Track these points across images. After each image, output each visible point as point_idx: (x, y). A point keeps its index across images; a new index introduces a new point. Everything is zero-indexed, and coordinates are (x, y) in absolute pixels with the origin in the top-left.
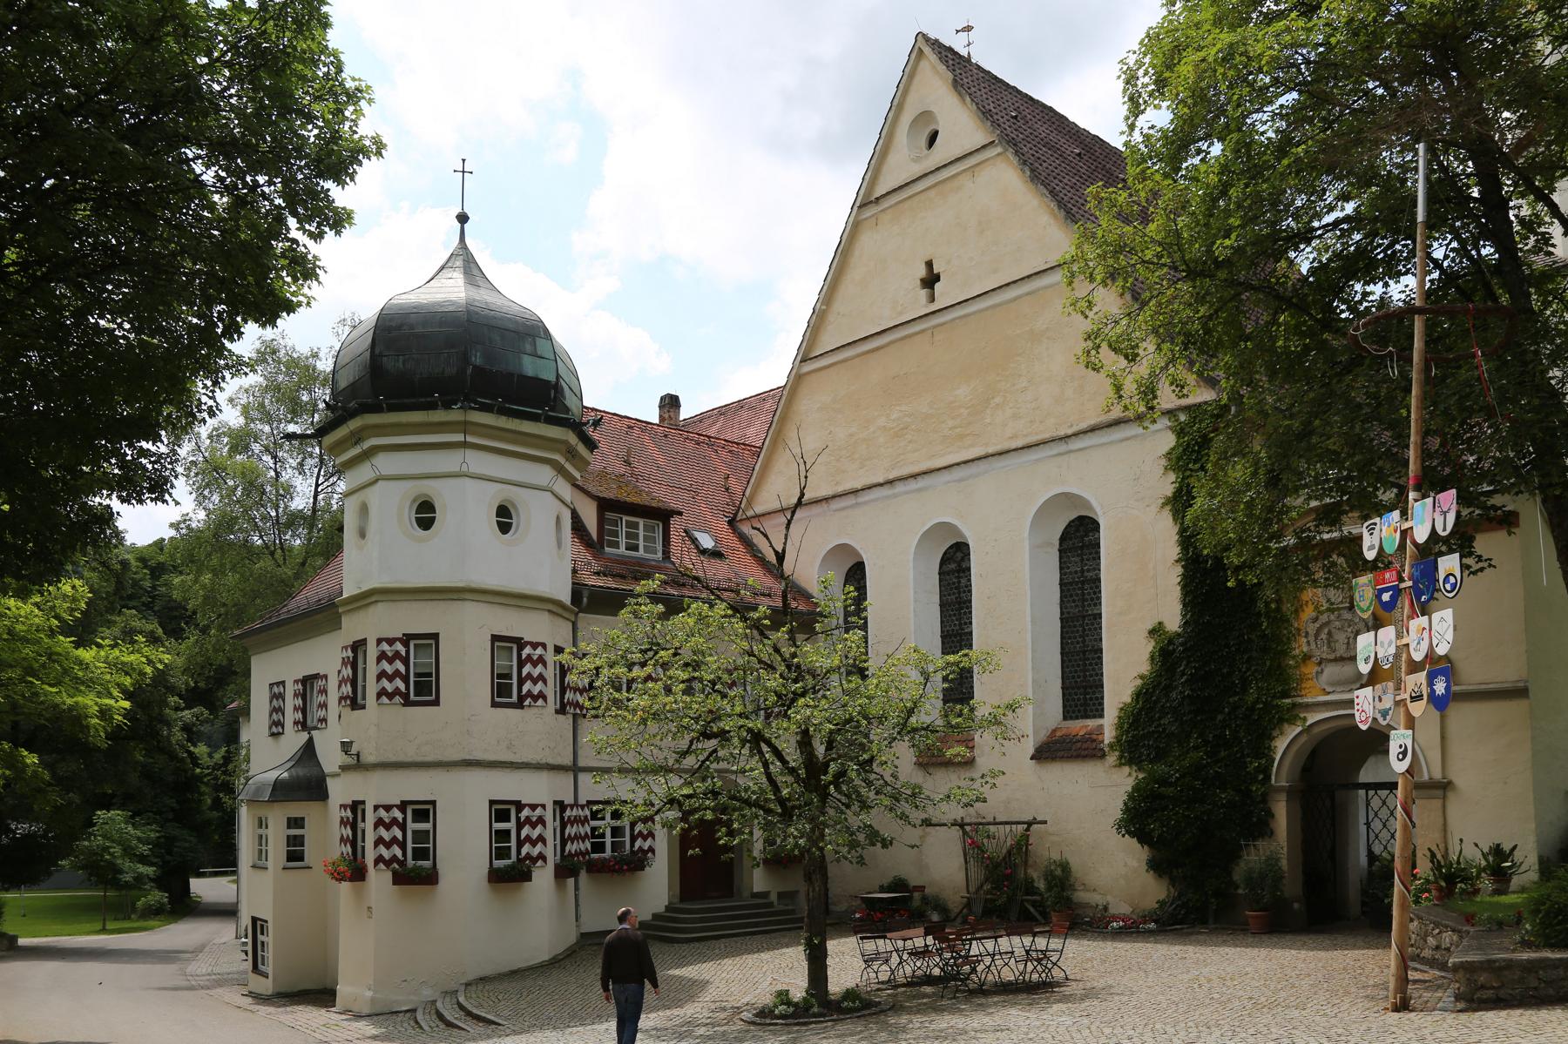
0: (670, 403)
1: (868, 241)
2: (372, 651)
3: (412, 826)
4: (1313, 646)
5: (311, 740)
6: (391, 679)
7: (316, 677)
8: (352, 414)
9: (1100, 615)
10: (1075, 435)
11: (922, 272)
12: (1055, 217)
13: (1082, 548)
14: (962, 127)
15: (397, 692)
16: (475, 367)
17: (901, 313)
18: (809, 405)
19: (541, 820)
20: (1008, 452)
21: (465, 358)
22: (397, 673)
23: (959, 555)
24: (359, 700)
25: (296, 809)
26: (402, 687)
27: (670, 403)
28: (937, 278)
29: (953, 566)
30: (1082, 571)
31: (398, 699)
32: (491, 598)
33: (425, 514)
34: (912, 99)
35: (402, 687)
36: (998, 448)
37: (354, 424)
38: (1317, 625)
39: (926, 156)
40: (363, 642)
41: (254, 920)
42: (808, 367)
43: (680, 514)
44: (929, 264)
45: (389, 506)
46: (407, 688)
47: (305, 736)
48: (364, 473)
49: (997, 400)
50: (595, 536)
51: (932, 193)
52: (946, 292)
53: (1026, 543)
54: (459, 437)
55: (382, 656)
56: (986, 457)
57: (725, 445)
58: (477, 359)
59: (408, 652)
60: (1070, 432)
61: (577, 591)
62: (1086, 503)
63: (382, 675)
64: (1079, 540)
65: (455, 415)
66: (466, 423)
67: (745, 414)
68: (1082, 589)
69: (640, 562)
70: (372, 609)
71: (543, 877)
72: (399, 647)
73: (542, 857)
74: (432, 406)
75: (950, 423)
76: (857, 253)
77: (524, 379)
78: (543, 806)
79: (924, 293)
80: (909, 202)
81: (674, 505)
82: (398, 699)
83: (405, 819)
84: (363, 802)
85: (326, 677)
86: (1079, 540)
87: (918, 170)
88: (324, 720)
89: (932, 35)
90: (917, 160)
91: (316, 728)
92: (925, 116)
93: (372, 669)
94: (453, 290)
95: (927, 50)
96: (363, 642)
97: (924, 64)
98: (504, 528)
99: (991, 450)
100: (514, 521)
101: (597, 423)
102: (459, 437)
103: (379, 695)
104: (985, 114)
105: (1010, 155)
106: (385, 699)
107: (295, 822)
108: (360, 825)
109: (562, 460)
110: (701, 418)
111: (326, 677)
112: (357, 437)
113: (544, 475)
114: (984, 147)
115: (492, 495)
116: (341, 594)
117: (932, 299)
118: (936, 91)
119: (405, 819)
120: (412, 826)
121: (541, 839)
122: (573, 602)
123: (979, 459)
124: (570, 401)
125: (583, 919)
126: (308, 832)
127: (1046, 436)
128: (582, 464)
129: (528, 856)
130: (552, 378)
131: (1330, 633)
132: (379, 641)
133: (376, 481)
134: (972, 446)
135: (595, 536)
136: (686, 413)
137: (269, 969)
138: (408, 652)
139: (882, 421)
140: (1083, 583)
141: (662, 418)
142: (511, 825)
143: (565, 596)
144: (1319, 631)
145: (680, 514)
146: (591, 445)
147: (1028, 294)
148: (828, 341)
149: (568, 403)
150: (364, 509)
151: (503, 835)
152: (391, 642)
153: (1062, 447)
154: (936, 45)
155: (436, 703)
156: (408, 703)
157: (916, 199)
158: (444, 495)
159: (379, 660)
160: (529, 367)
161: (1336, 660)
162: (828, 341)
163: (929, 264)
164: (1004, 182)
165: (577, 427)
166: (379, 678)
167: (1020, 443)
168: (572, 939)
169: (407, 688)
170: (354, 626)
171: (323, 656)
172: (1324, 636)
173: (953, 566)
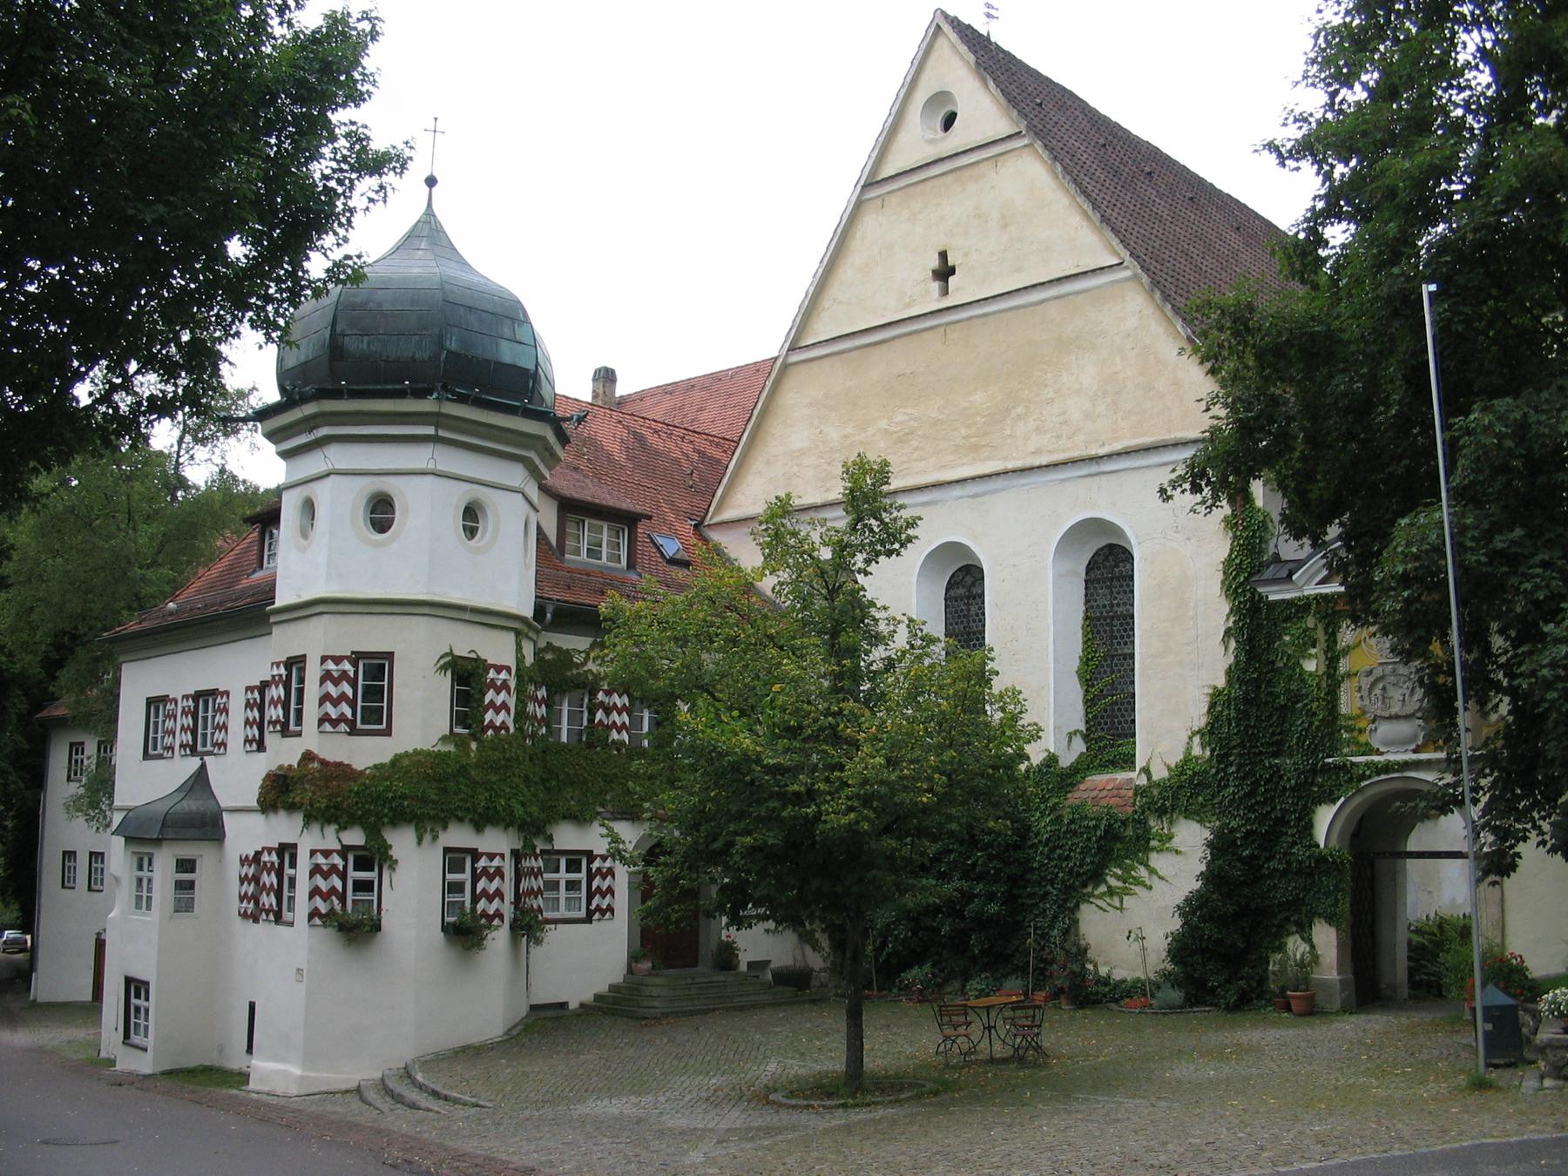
0: (606, 377)
1: (872, 225)
2: (313, 672)
3: (353, 875)
4: (1367, 702)
5: (203, 766)
6: (336, 703)
7: (213, 693)
8: (305, 399)
9: (1132, 656)
10: (1110, 456)
11: (935, 263)
12: (1088, 218)
13: (1112, 580)
14: (984, 114)
15: (342, 718)
16: (450, 352)
17: (908, 306)
18: (796, 397)
19: (499, 872)
20: (1031, 469)
21: (440, 342)
22: (343, 697)
23: (969, 579)
24: (292, 727)
25: (186, 851)
26: (348, 713)
27: (606, 377)
28: (952, 271)
29: (961, 591)
30: (1112, 605)
31: (343, 727)
32: (467, 616)
33: (381, 513)
34: (926, 77)
35: (348, 713)
36: (1019, 464)
37: (310, 409)
38: (1371, 679)
39: (943, 139)
40: (301, 659)
41: (129, 981)
42: (794, 358)
43: (650, 518)
44: (943, 255)
45: (340, 503)
46: (354, 714)
47: (195, 763)
48: (313, 464)
49: (1019, 410)
50: (553, 541)
51: (949, 179)
52: (962, 288)
53: (1050, 573)
54: (430, 430)
55: (326, 677)
56: (1006, 473)
57: (695, 436)
58: (453, 345)
59: (356, 672)
60: (1102, 452)
61: (539, 611)
62: (1118, 531)
63: (325, 698)
64: (1108, 568)
65: (427, 405)
66: (439, 414)
67: (697, 395)
68: (1111, 625)
69: (602, 572)
70: (314, 621)
71: (499, 939)
72: (347, 666)
73: (499, 915)
74: (400, 394)
75: (963, 431)
76: (859, 235)
77: (501, 366)
78: (502, 856)
79: (936, 286)
80: (921, 186)
81: (639, 509)
82: (343, 727)
83: (345, 867)
84: (295, 846)
85: (227, 693)
86: (1108, 568)
87: (932, 153)
88: (223, 744)
89: (952, 13)
90: (931, 142)
91: (210, 753)
92: (941, 97)
93: (312, 691)
94: (421, 268)
95: (946, 28)
96: (301, 659)
97: (941, 42)
98: (471, 532)
99: (1011, 465)
100: (480, 526)
101: (581, 420)
102: (430, 430)
103: (321, 721)
104: (1012, 100)
105: (1038, 145)
106: (327, 727)
107: (186, 865)
108: (288, 871)
109: (537, 461)
110: (641, 396)
111: (227, 693)
112: (309, 423)
113: (515, 475)
114: (1010, 137)
115: (460, 495)
116: (272, 600)
117: (945, 292)
118: (956, 74)
119: (345, 867)
120: (353, 875)
121: (499, 894)
122: (535, 617)
123: (998, 474)
124: (545, 392)
125: (533, 989)
126: (201, 877)
127: (1075, 454)
128: (551, 458)
129: (484, 914)
130: (531, 367)
131: (1384, 689)
132: (324, 659)
133: (328, 475)
134: (989, 458)
135: (553, 541)
136: (622, 389)
137: (150, 1042)
138: (356, 672)
139: (883, 424)
140: (1112, 618)
141: (595, 395)
142: (466, 876)
143: (528, 612)
144: (1373, 685)
145: (650, 518)
146: (563, 439)
147: (1057, 298)
148: (824, 328)
149: (544, 393)
150: (309, 507)
151: (456, 888)
152: (338, 660)
153: (1094, 468)
154: (955, 23)
155: (388, 732)
156: (354, 732)
157: (930, 184)
158: (407, 494)
159: (322, 681)
160: (507, 354)
161: (1390, 718)
162: (824, 328)
163: (943, 255)
164: (1030, 177)
165: (556, 423)
166: (322, 702)
167: (1044, 460)
168: (523, 1011)
169: (354, 714)
170: (285, 641)
171: (237, 668)
172: (1377, 691)
173: (961, 591)
